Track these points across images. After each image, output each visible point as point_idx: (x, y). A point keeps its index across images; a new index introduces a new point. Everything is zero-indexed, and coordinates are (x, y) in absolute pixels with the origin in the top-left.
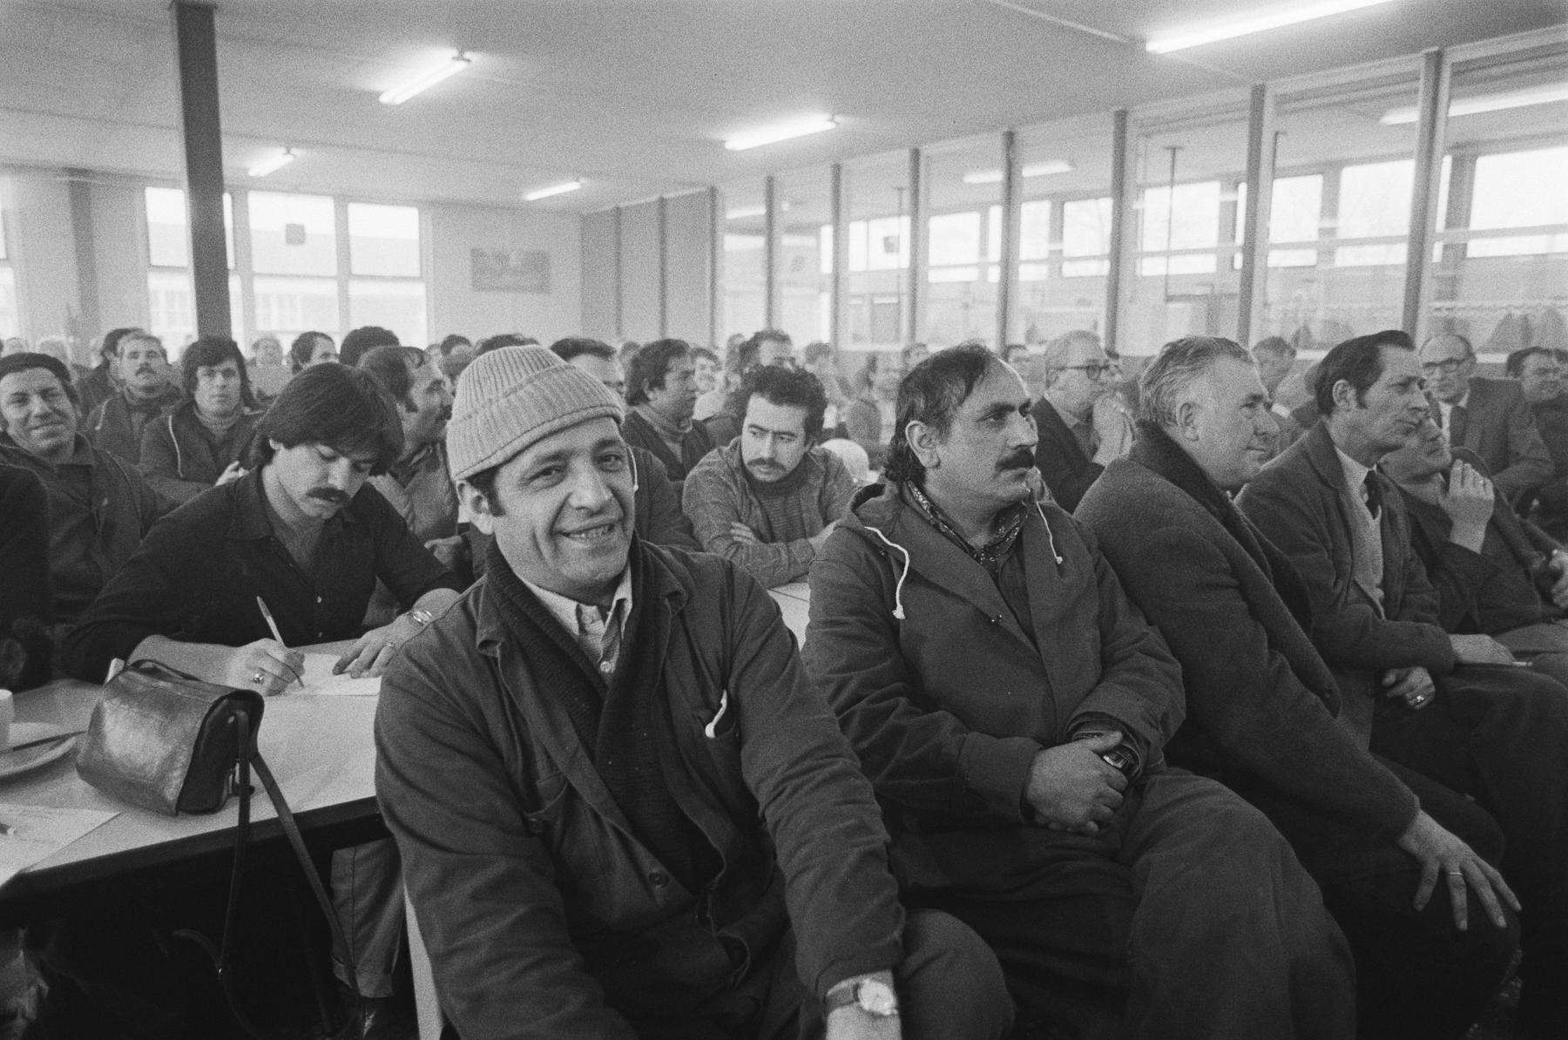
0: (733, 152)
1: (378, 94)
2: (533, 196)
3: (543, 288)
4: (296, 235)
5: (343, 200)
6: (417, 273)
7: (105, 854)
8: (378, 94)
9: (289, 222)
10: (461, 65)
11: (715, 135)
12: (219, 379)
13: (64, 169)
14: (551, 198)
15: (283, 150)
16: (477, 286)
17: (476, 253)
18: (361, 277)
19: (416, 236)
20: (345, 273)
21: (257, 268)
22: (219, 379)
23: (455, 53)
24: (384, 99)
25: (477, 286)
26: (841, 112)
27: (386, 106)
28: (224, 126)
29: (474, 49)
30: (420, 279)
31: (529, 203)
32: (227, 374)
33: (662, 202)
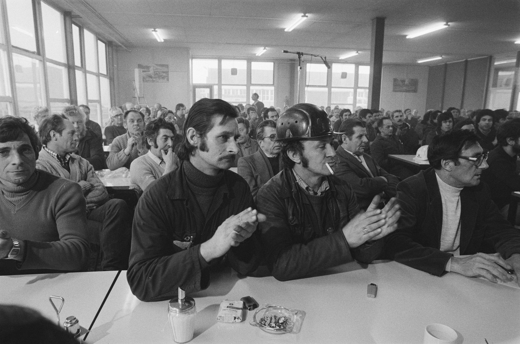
0: (409, 39)
1: (284, 29)
2: (420, 62)
3: (415, 91)
4: (234, 72)
5: (220, 59)
6: (325, 84)
7: (353, 272)
8: (284, 29)
9: (343, 72)
10: (305, 18)
11: (512, 40)
12: (448, 123)
13: (290, 60)
14: (499, 65)
15: (356, 52)
16: (394, 91)
17: (395, 80)
18: (308, 86)
19: (246, 69)
20: (249, 83)
21: (333, 86)
22: (448, 123)
23: (303, 14)
24: (286, 30)
25: (394, 91)
26: (451, 21)
27: (287, 32)
28: (384, 49)
29: (309, 13)
30: (273, 85)
31: (419, 63)
32: (450, 122)
33: (466, 61)
